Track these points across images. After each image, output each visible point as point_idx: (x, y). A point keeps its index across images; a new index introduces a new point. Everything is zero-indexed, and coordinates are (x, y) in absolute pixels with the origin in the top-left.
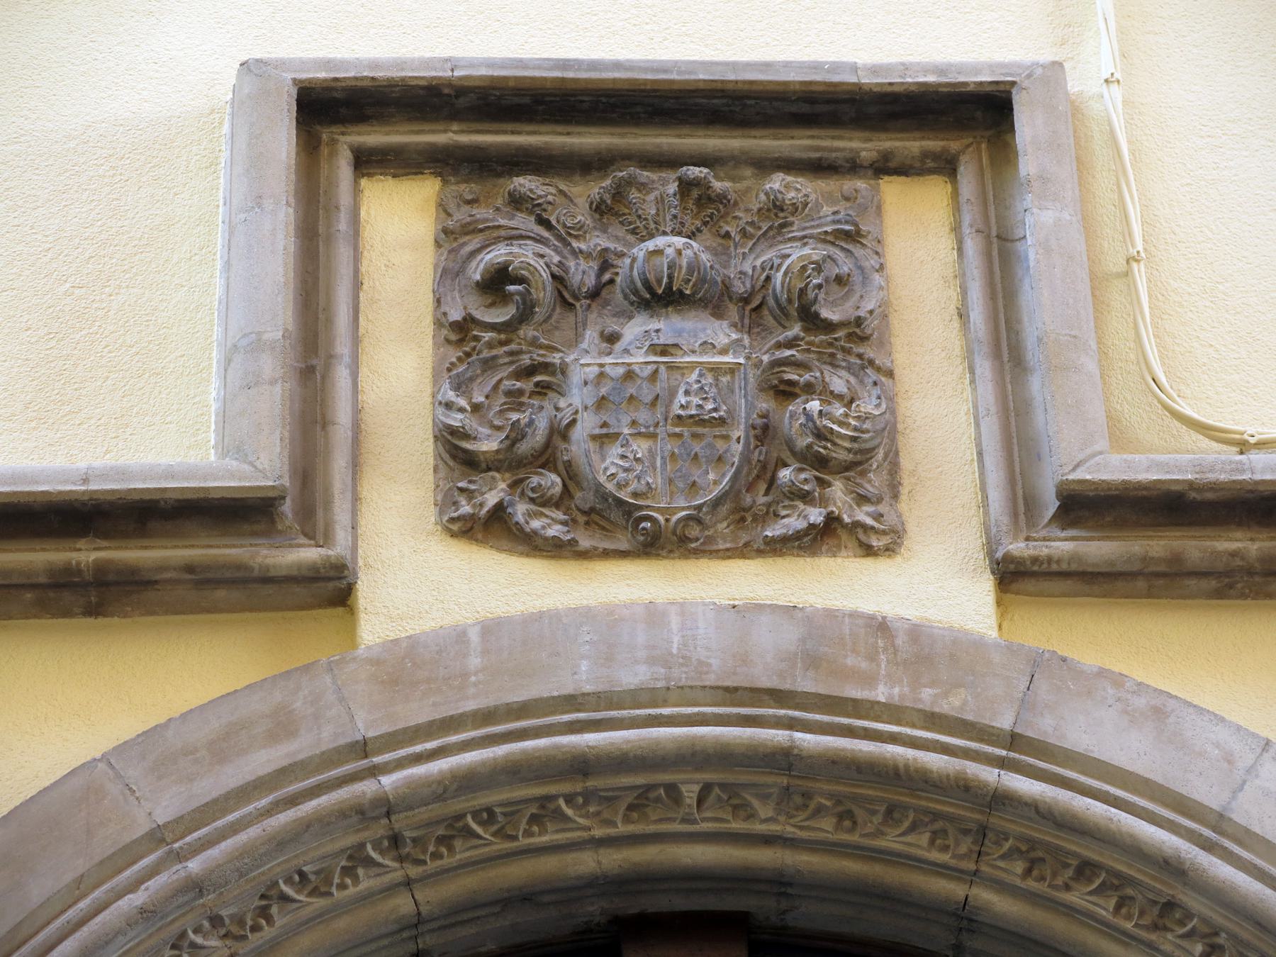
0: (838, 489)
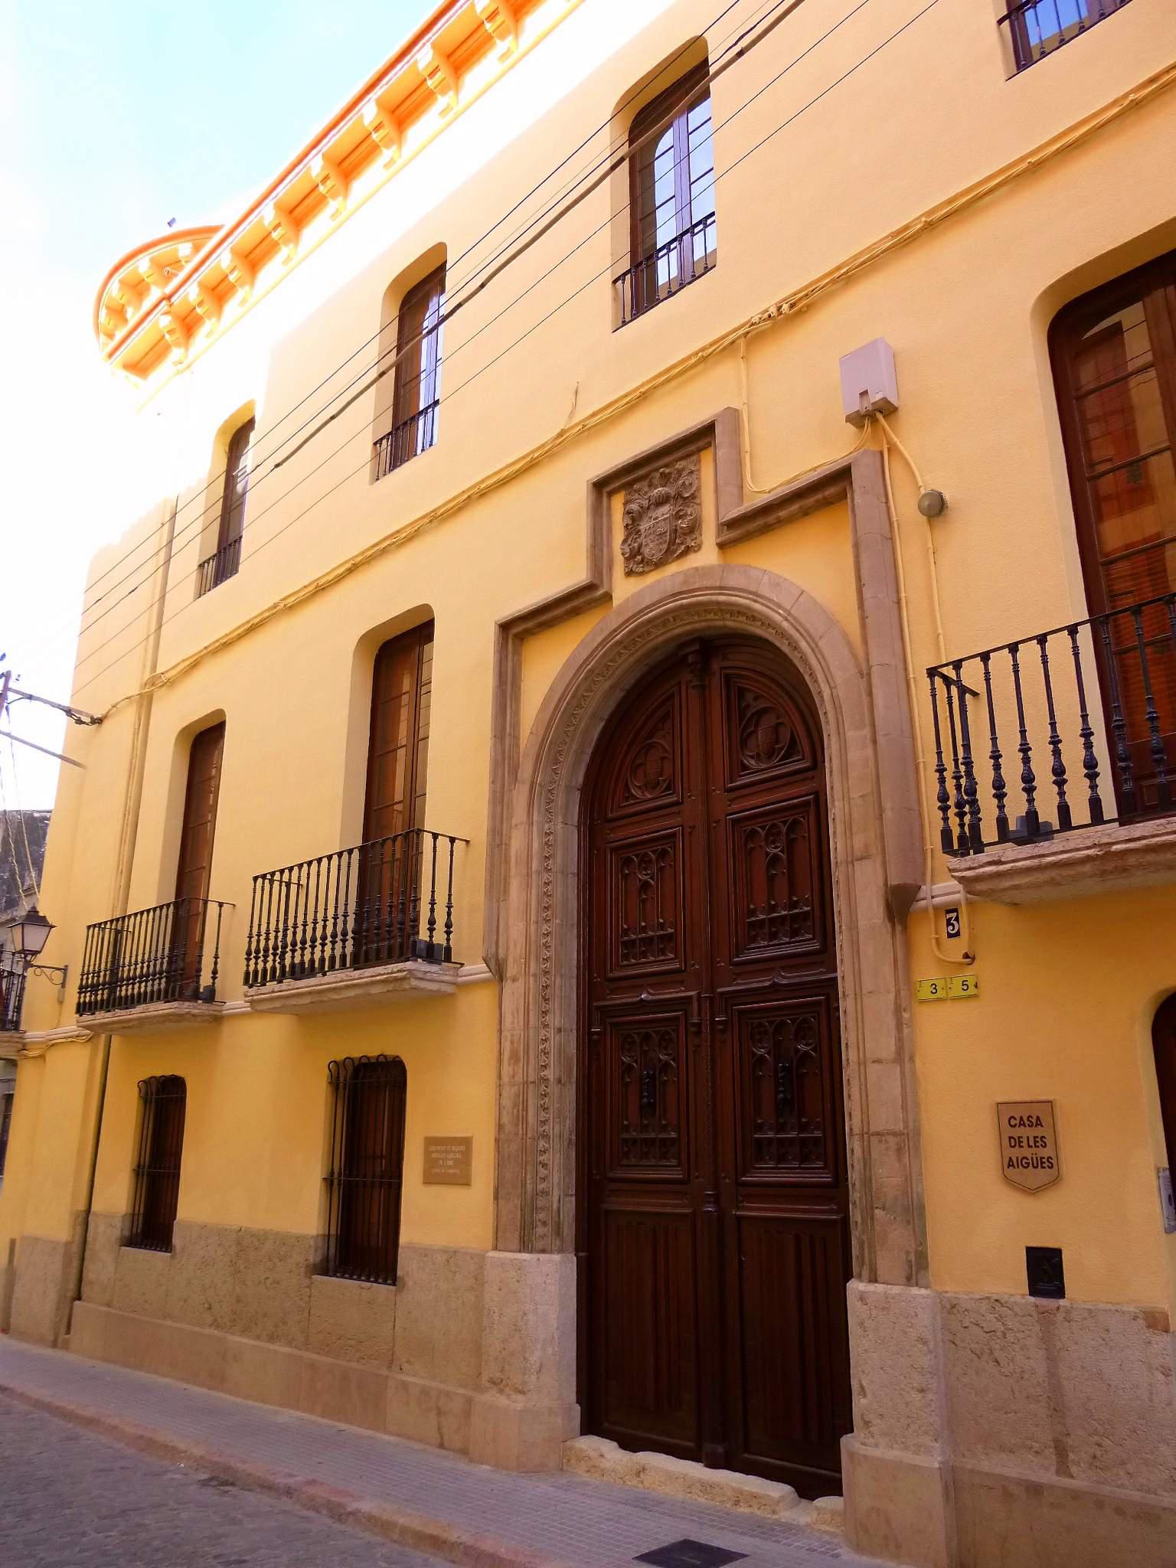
0: (688, 539)
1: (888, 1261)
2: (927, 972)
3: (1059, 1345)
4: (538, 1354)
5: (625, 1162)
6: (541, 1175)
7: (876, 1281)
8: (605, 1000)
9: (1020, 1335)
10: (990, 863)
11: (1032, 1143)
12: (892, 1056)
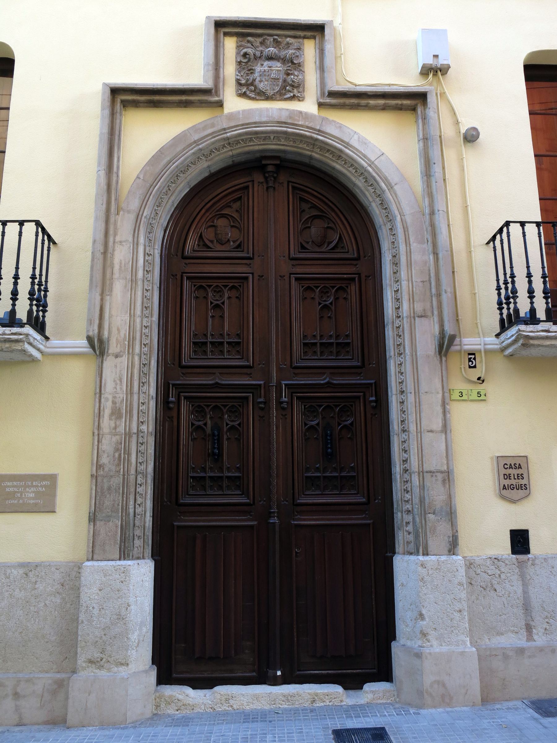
0: (295, 90)
2: (458, 385)
3: (529, 577)
4: (136, 634)
7: (428, 555)
8: (179, 380)
9: (509, 575)
10: (543, 331)
11: (516, 477)
12: (440, 429)
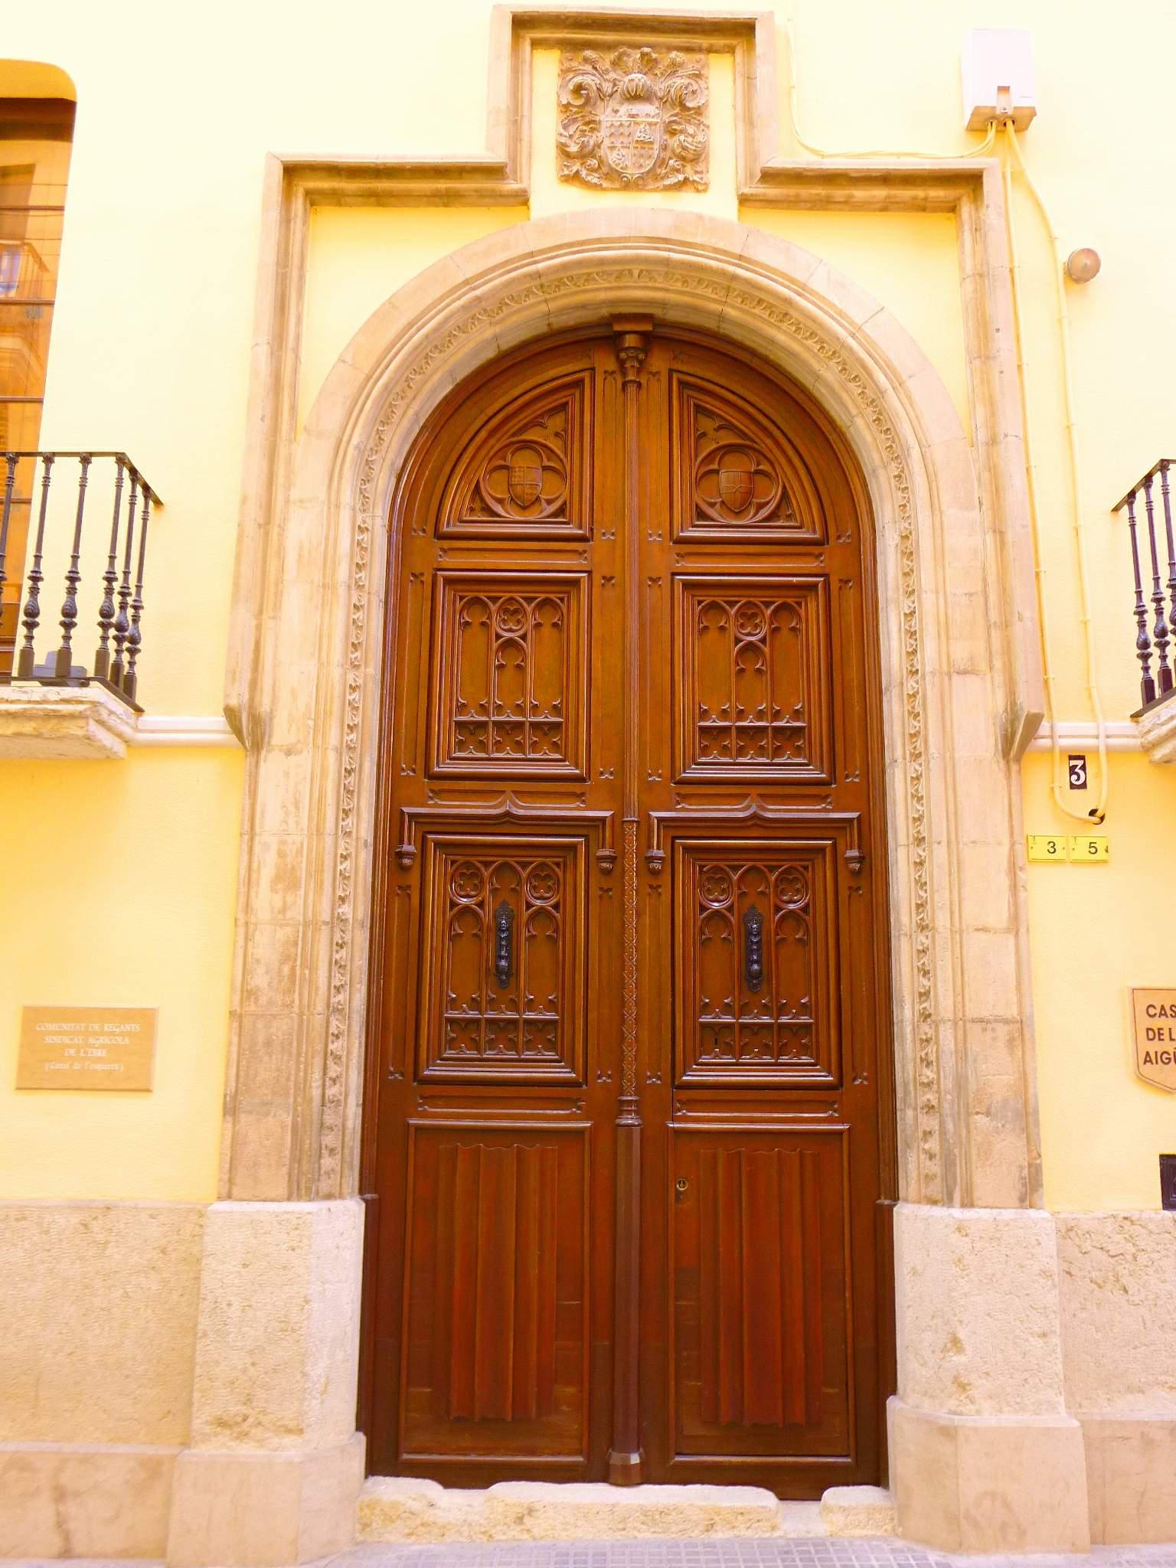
1: (993, 1176)
5: (705, 1059)
6: (332, 1074)
7: (972, 1205)
9: (1156, 1256)
12: (1004, 924)
